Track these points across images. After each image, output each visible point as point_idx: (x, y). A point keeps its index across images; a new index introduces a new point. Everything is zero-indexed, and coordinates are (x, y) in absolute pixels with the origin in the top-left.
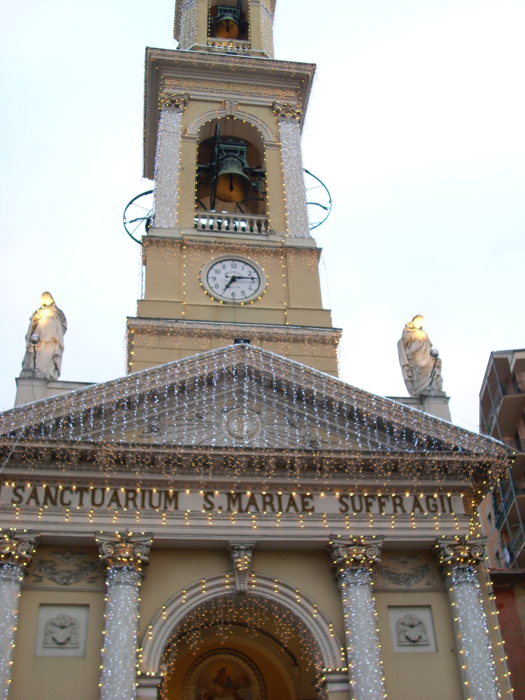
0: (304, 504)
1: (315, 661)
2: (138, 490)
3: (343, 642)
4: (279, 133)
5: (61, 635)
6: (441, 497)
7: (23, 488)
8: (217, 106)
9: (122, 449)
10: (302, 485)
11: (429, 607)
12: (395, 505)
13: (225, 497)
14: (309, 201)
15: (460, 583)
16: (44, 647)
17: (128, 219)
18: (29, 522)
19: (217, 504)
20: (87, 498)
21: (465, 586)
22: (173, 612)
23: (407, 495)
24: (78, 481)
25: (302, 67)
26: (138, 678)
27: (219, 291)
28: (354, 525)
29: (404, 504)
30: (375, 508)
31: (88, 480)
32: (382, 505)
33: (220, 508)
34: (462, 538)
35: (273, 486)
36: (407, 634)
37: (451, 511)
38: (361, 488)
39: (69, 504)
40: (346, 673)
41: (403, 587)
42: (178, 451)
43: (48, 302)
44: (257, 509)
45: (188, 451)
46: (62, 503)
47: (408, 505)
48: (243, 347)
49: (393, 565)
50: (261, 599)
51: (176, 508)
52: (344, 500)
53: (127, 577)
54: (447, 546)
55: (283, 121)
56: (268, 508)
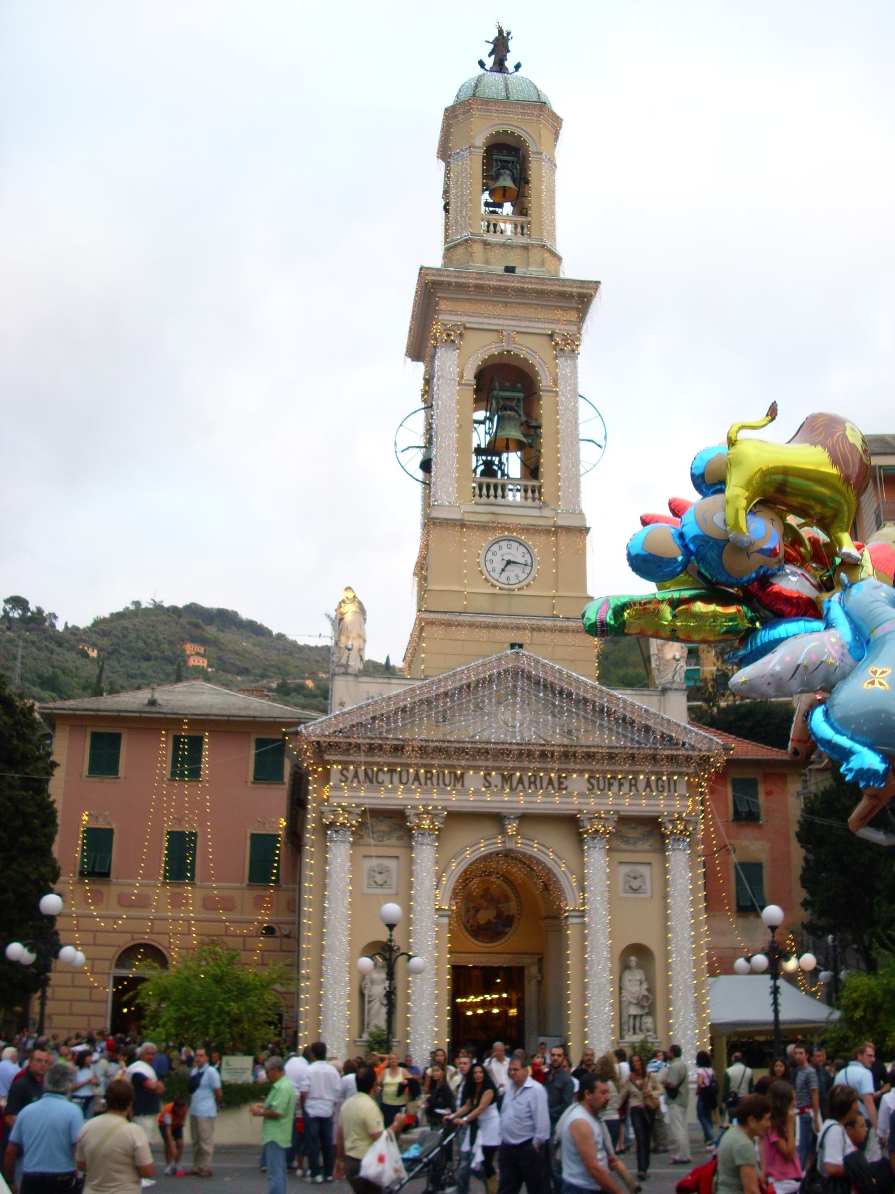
0: (560, 783)
1: (561, 902)
2: (434, 771)
3: (583, 889)
4: (557, 374)
5: (379, 879)
6: (669, 779)
7: (347, 770)
8: (493, 337)
9: (424, 744)
11: (650, 864)
12: (631, 785)
13: (499, 778)
14: (581, 437)
15: (674, 850)
17: (401, 447)
18: (354, 797)
20: (396, 777)
21: (677, 852)
22: (459, 863)
23: (642, 777)
24: (388, 764)
26: (437, 910)
27: (496, 575)
28: (598, 801)
29: (638, 785)
30: (615, 787)
31: (396, 764)
32: (620, 784)
33: (496, 786)
34: (680, 814)
36: (631, 884)
38: (605, 772)
39: (382, 783)
40: (583, 911)
41: (631, 847)
42: (467, 745)
43: (350, 595)
44: (524, 787)
45: (474, 746)
46: (378, 782)
47: (641, 786)
48: (518, 653)
49: (625, 830)
50: (524, 854)
51: (463, 785)
52: (592, 780)
53: (428, 840)
55: (562, 356)
56: (532, 786)
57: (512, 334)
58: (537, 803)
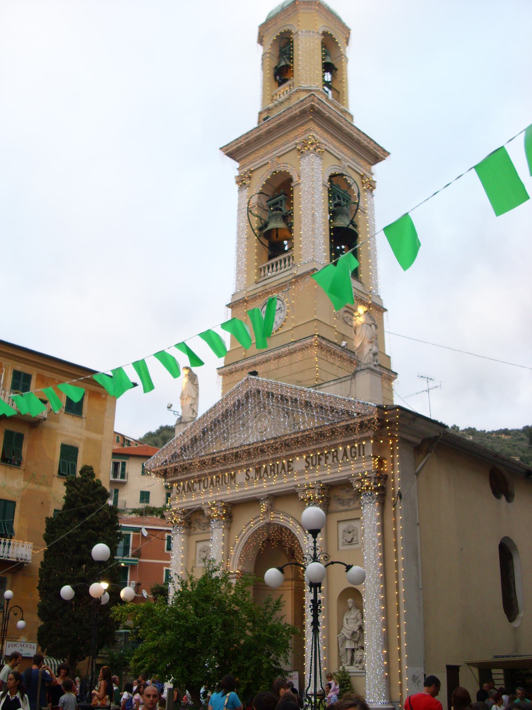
0: (289, 466)
6: (359, 446)
10: (246, 465)
12: (333, 457)
16: (343, 545)
19: (251, 476)
25: (240, 140)
32: (327, 458)
34: (308, 484)
35: (274, 460)
37: (364, 455)
38: (314, 451)
41: (346, 507)
46: (194, 490)
54: (354, 481)
57: (274, 160)
58: (283, 483)
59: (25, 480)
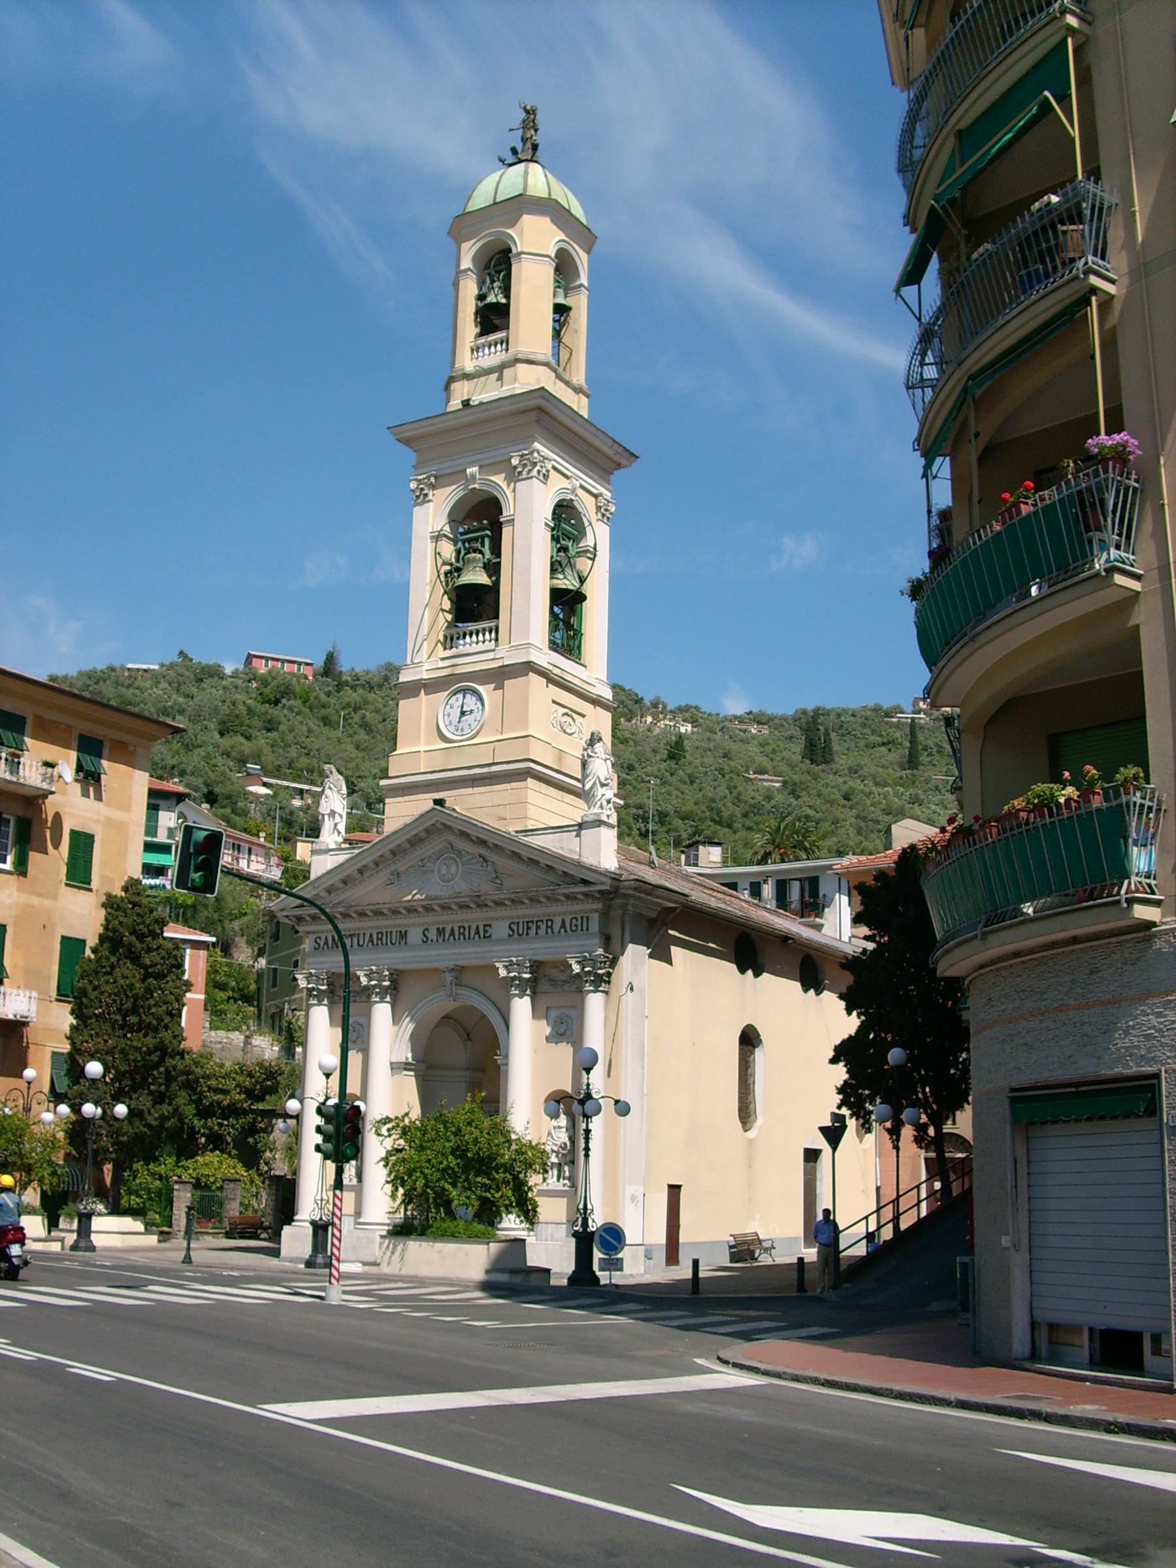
0: (485, 931)
59: (19, 890)
